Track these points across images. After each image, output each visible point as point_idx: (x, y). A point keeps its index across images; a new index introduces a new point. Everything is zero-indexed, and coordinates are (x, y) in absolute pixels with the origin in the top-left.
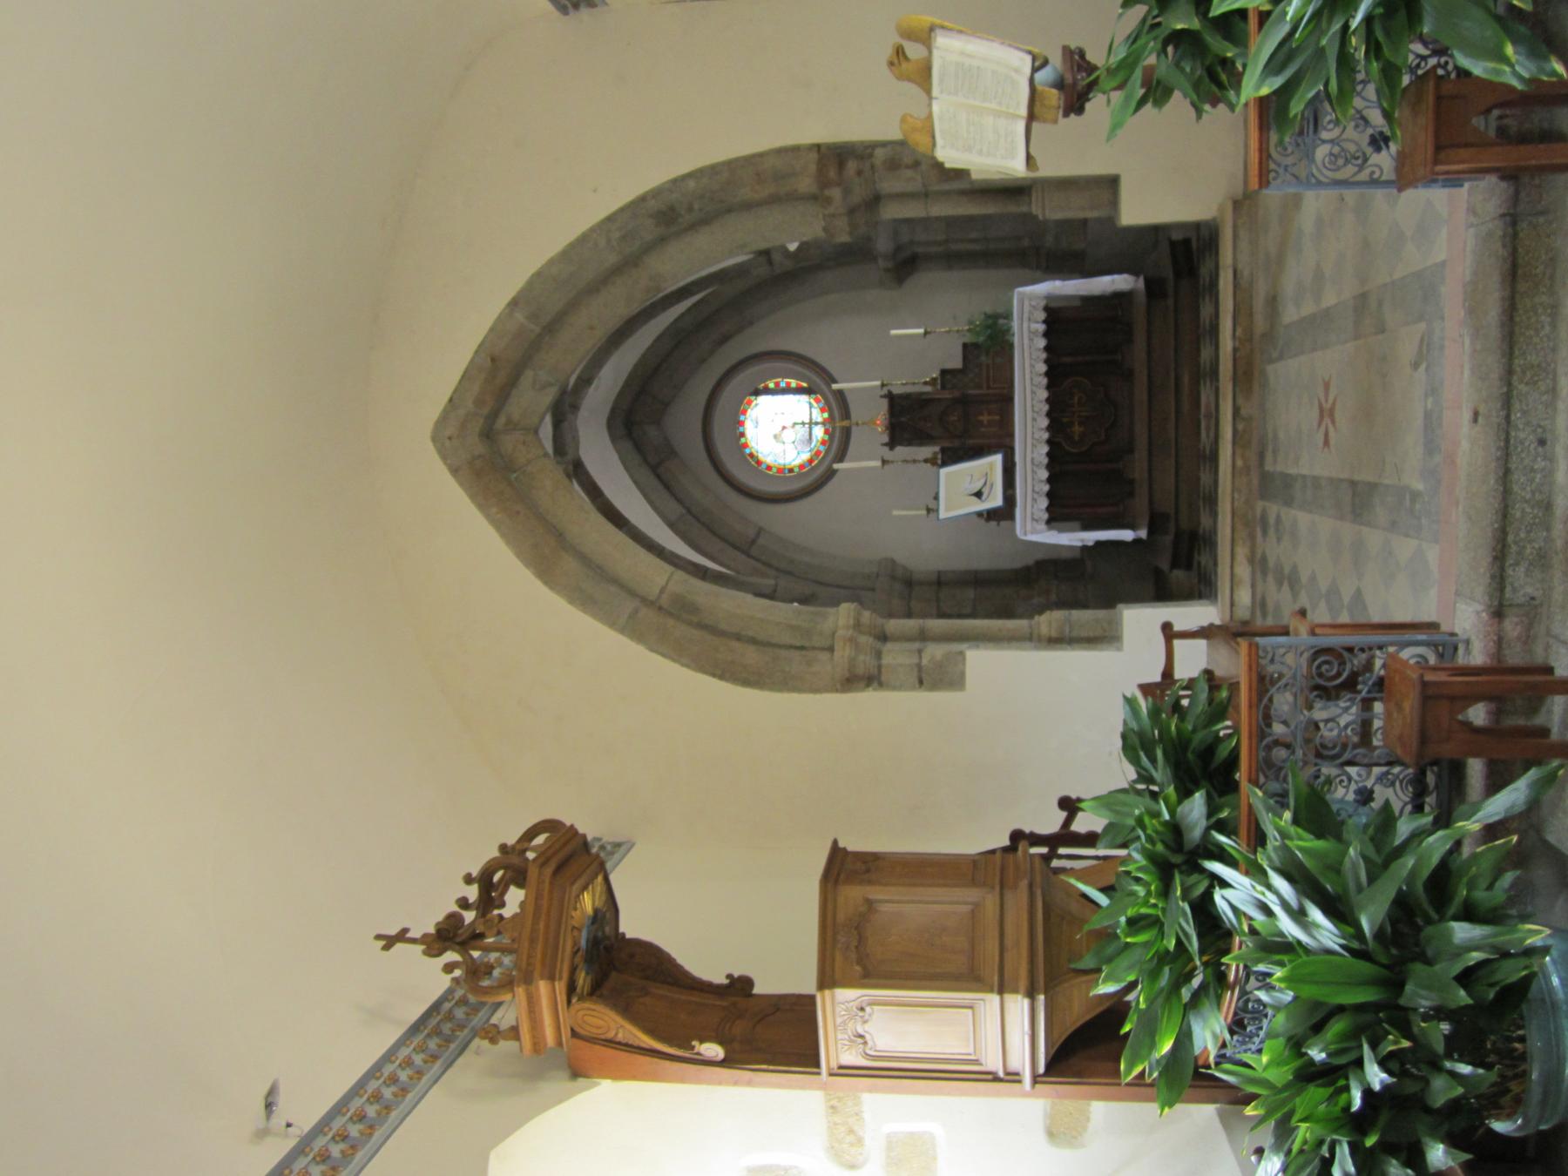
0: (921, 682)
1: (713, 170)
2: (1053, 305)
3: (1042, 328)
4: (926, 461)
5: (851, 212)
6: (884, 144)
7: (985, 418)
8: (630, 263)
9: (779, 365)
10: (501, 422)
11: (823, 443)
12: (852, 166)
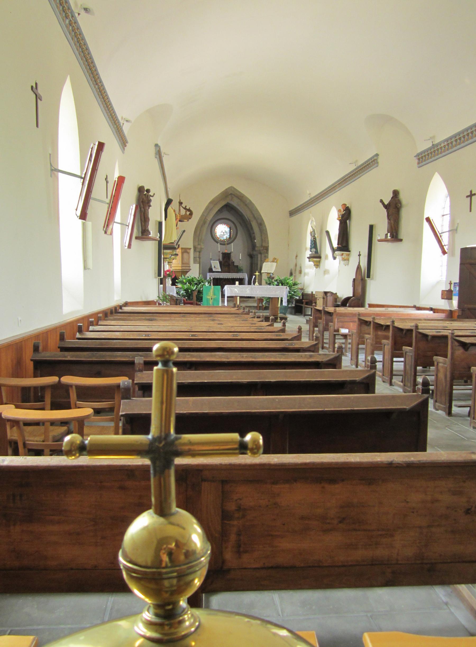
0: (194, 258)
1: (266, 231)
2: (244, 280)
3: (241, 278)
4: (219, 259)
5: (260, 250)
6: (268, 255)
7: (226, 268)
8: (255, 218)
9: (235, 233)
10: (233, 196)
11: (221, 240)
12: (265, 251)
